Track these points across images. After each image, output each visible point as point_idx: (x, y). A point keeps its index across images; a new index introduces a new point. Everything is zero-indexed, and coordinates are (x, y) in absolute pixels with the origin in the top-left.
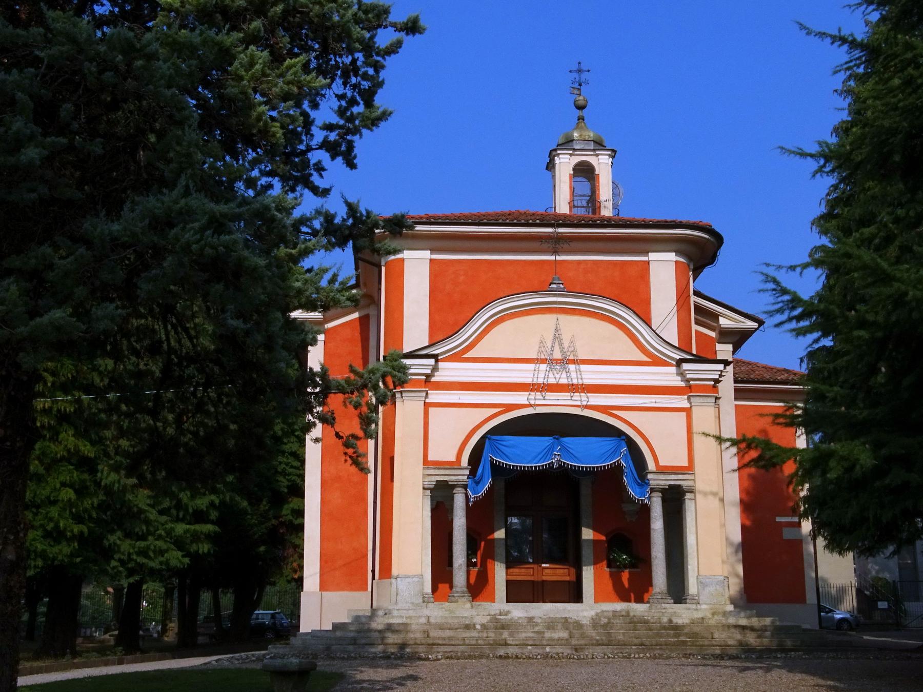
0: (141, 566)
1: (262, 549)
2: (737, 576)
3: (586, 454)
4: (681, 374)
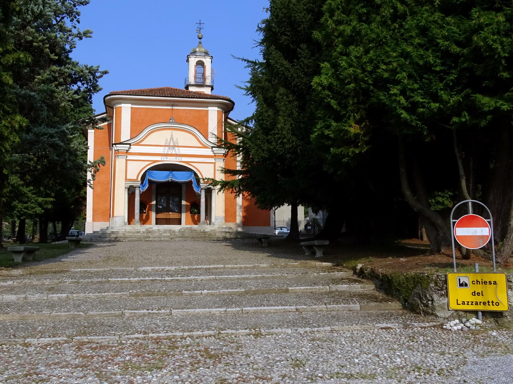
0: (26, 213)
1: (73, 206)
2: (240, 216)
3: (180, 177)
4: (213, 151)
